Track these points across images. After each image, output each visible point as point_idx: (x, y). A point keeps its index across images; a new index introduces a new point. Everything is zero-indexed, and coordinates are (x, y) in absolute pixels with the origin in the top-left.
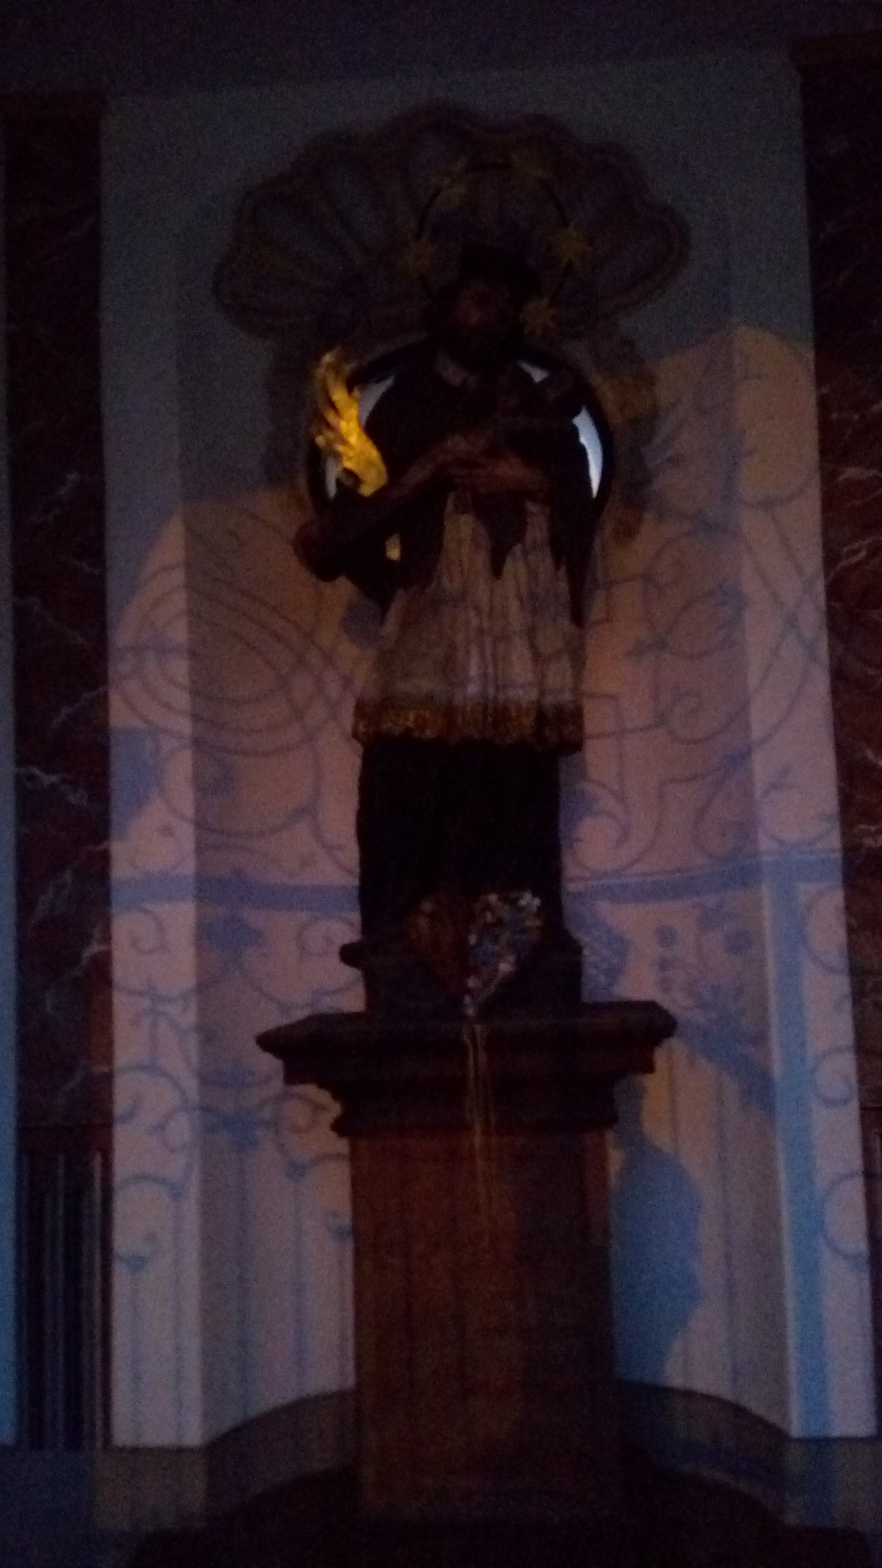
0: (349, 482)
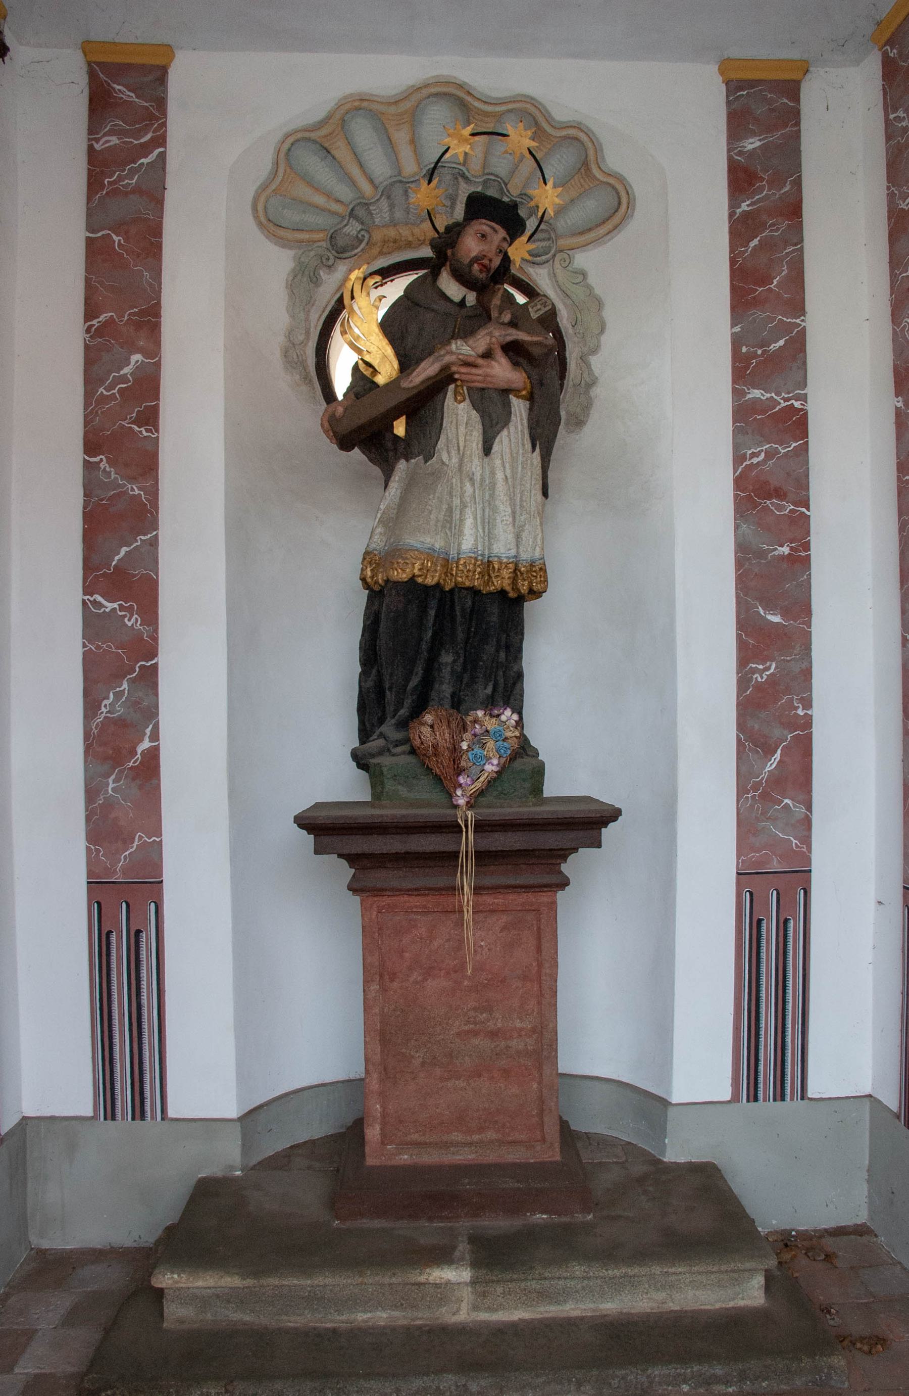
0: (367, 372)
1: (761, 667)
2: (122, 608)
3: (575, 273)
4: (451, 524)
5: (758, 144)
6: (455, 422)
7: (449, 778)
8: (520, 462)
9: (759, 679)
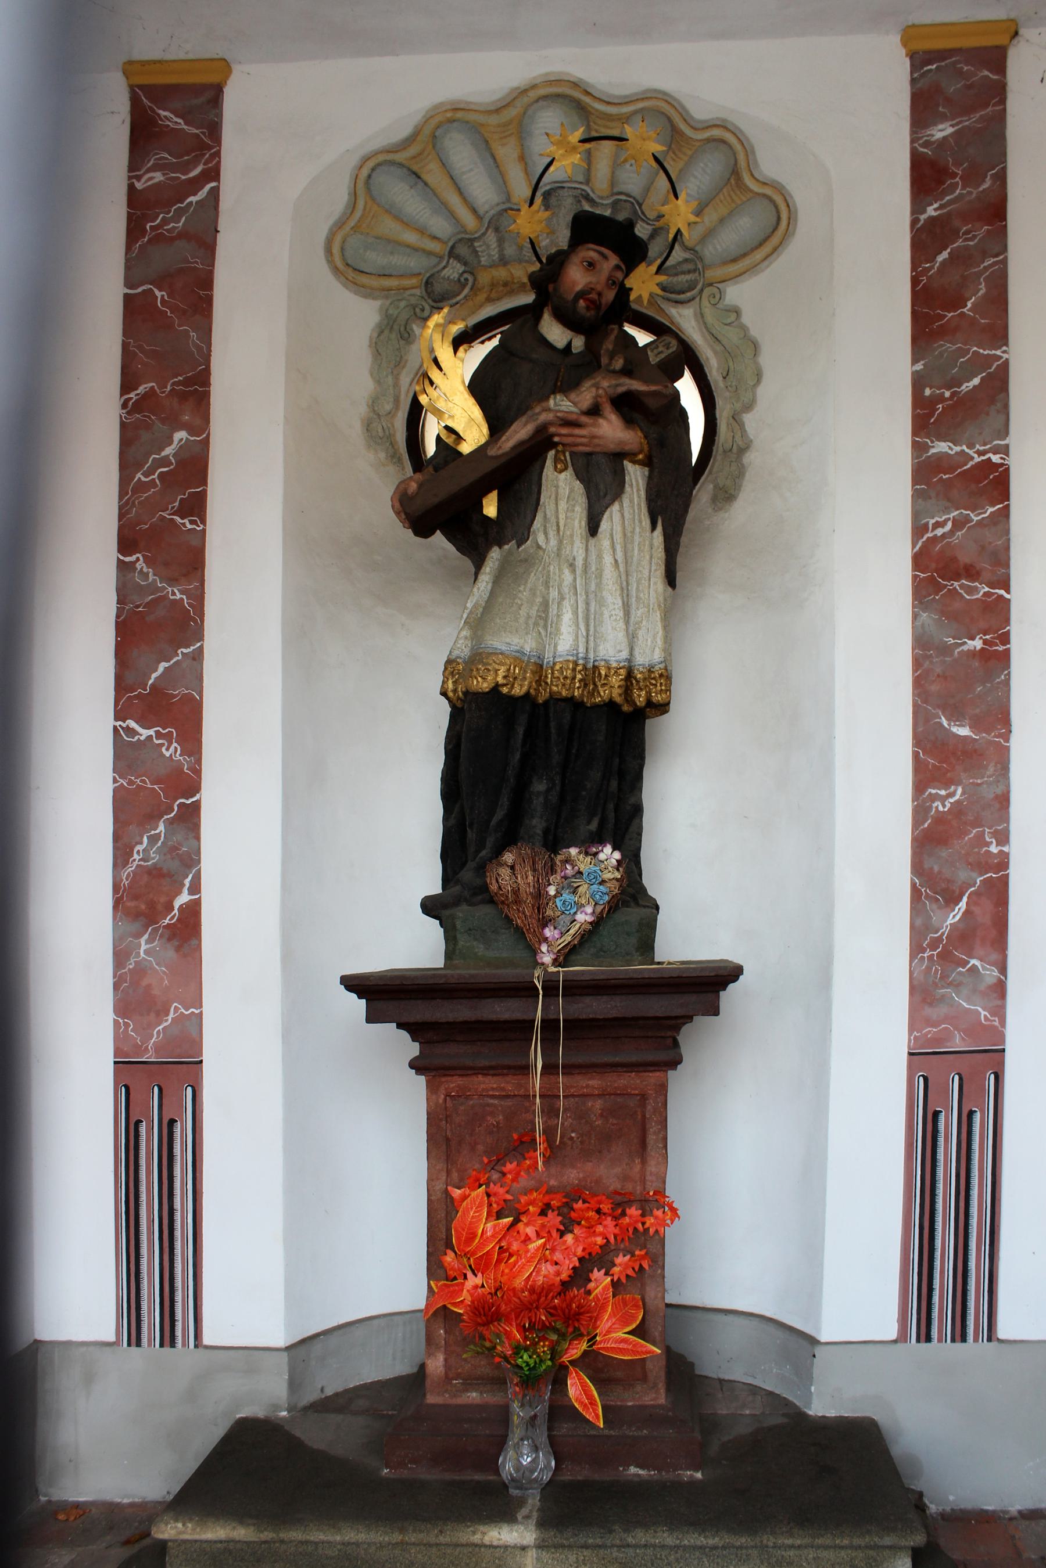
0: (449, 440)
1: (943, 793)
2: (159, 735)
3: (727, 311)
4: (546, 621)
5: (950, 130)
6: (553, 496)
7: (532, 930)
8: (636, 544)
9: (941, 808)
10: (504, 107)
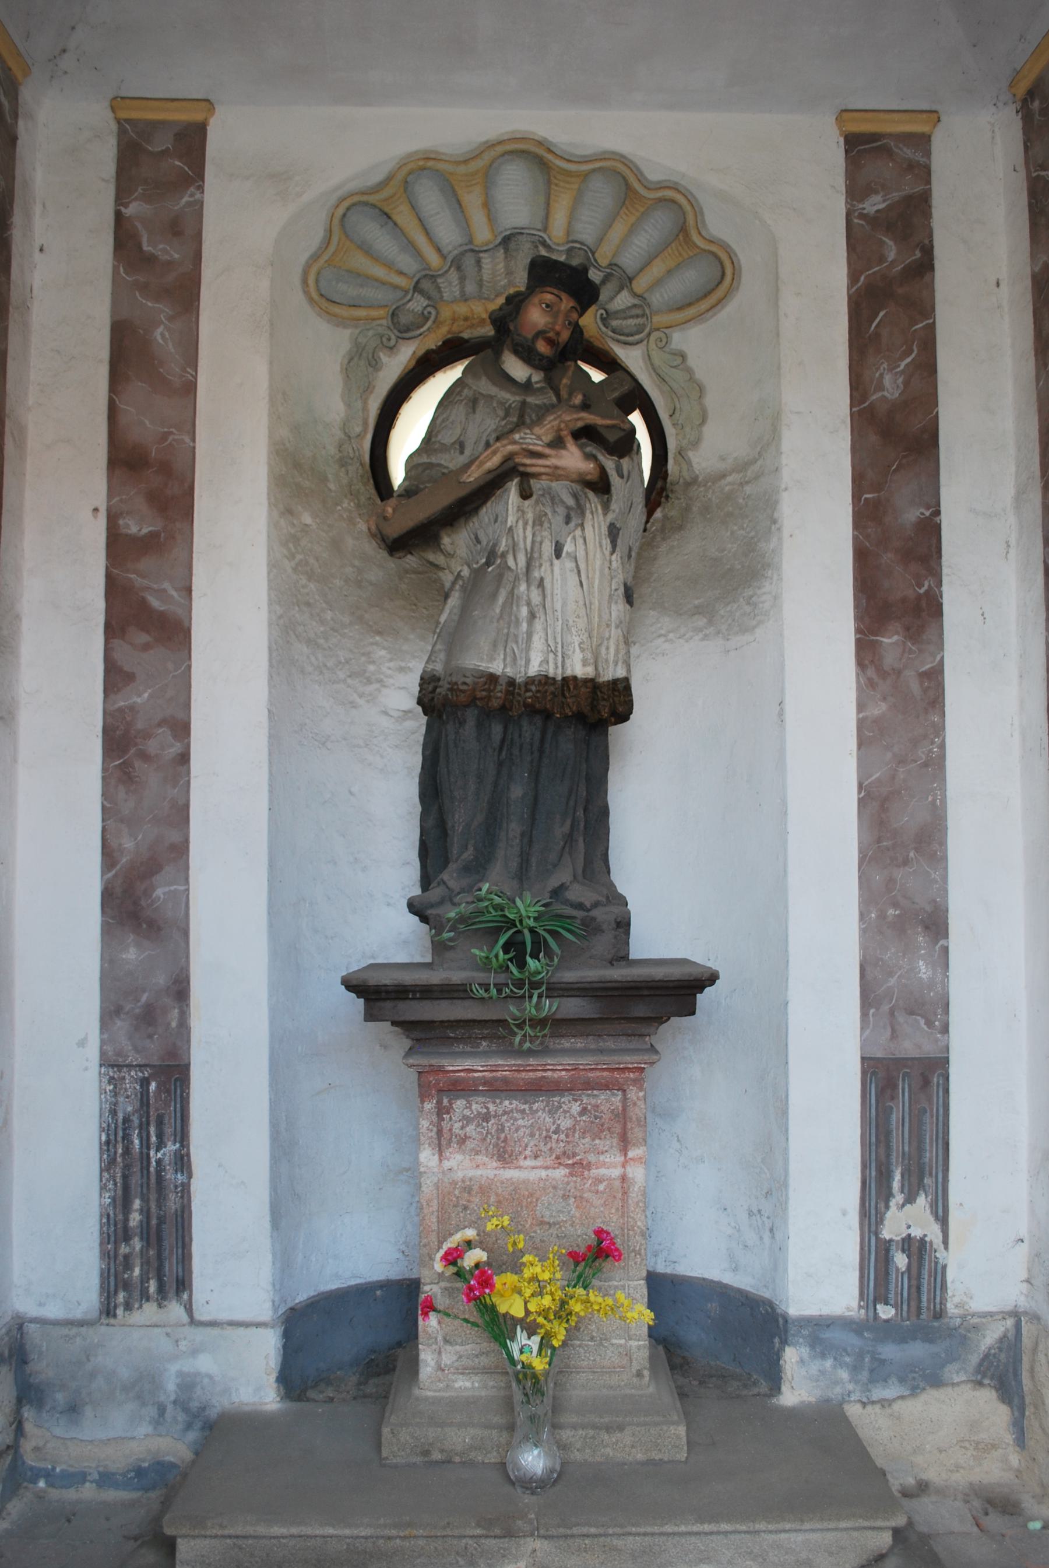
3: (675, 354)
10: (472, 158)
